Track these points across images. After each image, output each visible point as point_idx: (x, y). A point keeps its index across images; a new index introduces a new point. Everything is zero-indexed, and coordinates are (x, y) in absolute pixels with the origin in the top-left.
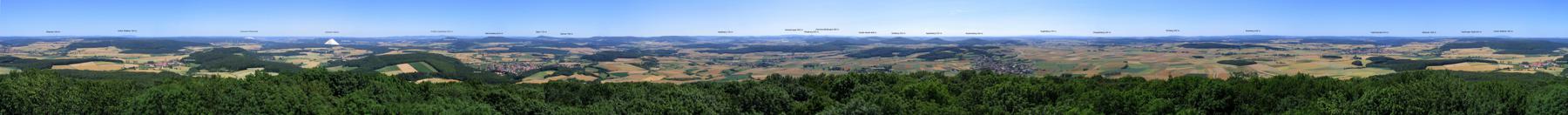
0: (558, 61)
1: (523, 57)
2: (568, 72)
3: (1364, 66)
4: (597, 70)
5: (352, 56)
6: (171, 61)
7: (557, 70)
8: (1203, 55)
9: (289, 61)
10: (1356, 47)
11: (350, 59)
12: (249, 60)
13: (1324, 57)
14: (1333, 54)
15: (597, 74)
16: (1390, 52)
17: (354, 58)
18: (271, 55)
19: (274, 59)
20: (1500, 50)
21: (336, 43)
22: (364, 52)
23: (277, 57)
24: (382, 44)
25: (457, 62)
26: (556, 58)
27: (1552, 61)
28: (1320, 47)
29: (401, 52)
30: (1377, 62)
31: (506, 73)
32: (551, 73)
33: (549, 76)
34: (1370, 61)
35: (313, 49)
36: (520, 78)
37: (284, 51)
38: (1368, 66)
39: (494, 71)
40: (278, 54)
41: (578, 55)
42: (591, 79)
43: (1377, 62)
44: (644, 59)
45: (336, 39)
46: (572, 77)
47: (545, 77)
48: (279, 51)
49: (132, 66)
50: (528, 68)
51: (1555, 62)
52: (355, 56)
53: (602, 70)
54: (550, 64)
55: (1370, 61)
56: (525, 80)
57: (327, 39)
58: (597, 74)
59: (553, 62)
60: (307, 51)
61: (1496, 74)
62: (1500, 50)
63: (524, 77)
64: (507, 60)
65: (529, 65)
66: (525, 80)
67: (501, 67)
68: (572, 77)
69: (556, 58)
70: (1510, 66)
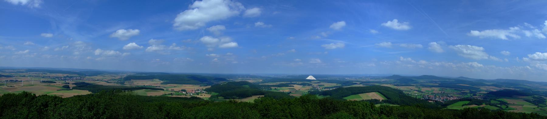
0: (472, 95)
1: (448, 91)
2: (479, 103)
3: (71, 88)
4: (499, 103)
5: (326, 88)
6: (198, 90)
7: (471, 101)
8: (56, 82)
9: (281, 91)
10: (65, 75)
11: (324, 90)
12: (255, 90)
13: (44, 82)
14: (49, 80)
15: (499, 105)
16: (87, 80)
17: (327, 89)
18: (269, 86)
19: (271, 89)
20: (166, 81)
21: (313, 78)
22: (335, 85)
23: (273, 88)
24: (348, 79)
25: (400, 92)
26: (471, 92)
27: (203, 90)
28: (41, 75)
29: (361, 85)
30: (81, 86)
31: (436, 101)
32: (467, 102)
33: (466, 105)
34: (75, 85)
35: (297, 82)
36: (445, 105)
37: (278, 83)
38: (74, 88)
39: (427, 100)
40: (274, 86)
41: (486, 91)
42: (495, 108)
43: (81, 86)
44: (534, 98)
45: (314, 76)
46: (481, 106)
47: (463, 106)
48: (274, 84)
49: (170, 93)
50: (452, 99)
51: (205, 90)
52: (328, 88)
53: (502, 103)
54: (466, 96)
55: (75, 85)
56: (449, 107)
57: (308, 76)
58: (499, 105)
59: (469, 96)
60: (294, 84)
61: (163, 98)
62: (166, 81)
63: (448, 105)
64: (436, 92)
65: (452, 96)
66: (449, 107)
67: (432, 97)
68: (481, 106)
69: (471, 92)
70: (172, 92)
